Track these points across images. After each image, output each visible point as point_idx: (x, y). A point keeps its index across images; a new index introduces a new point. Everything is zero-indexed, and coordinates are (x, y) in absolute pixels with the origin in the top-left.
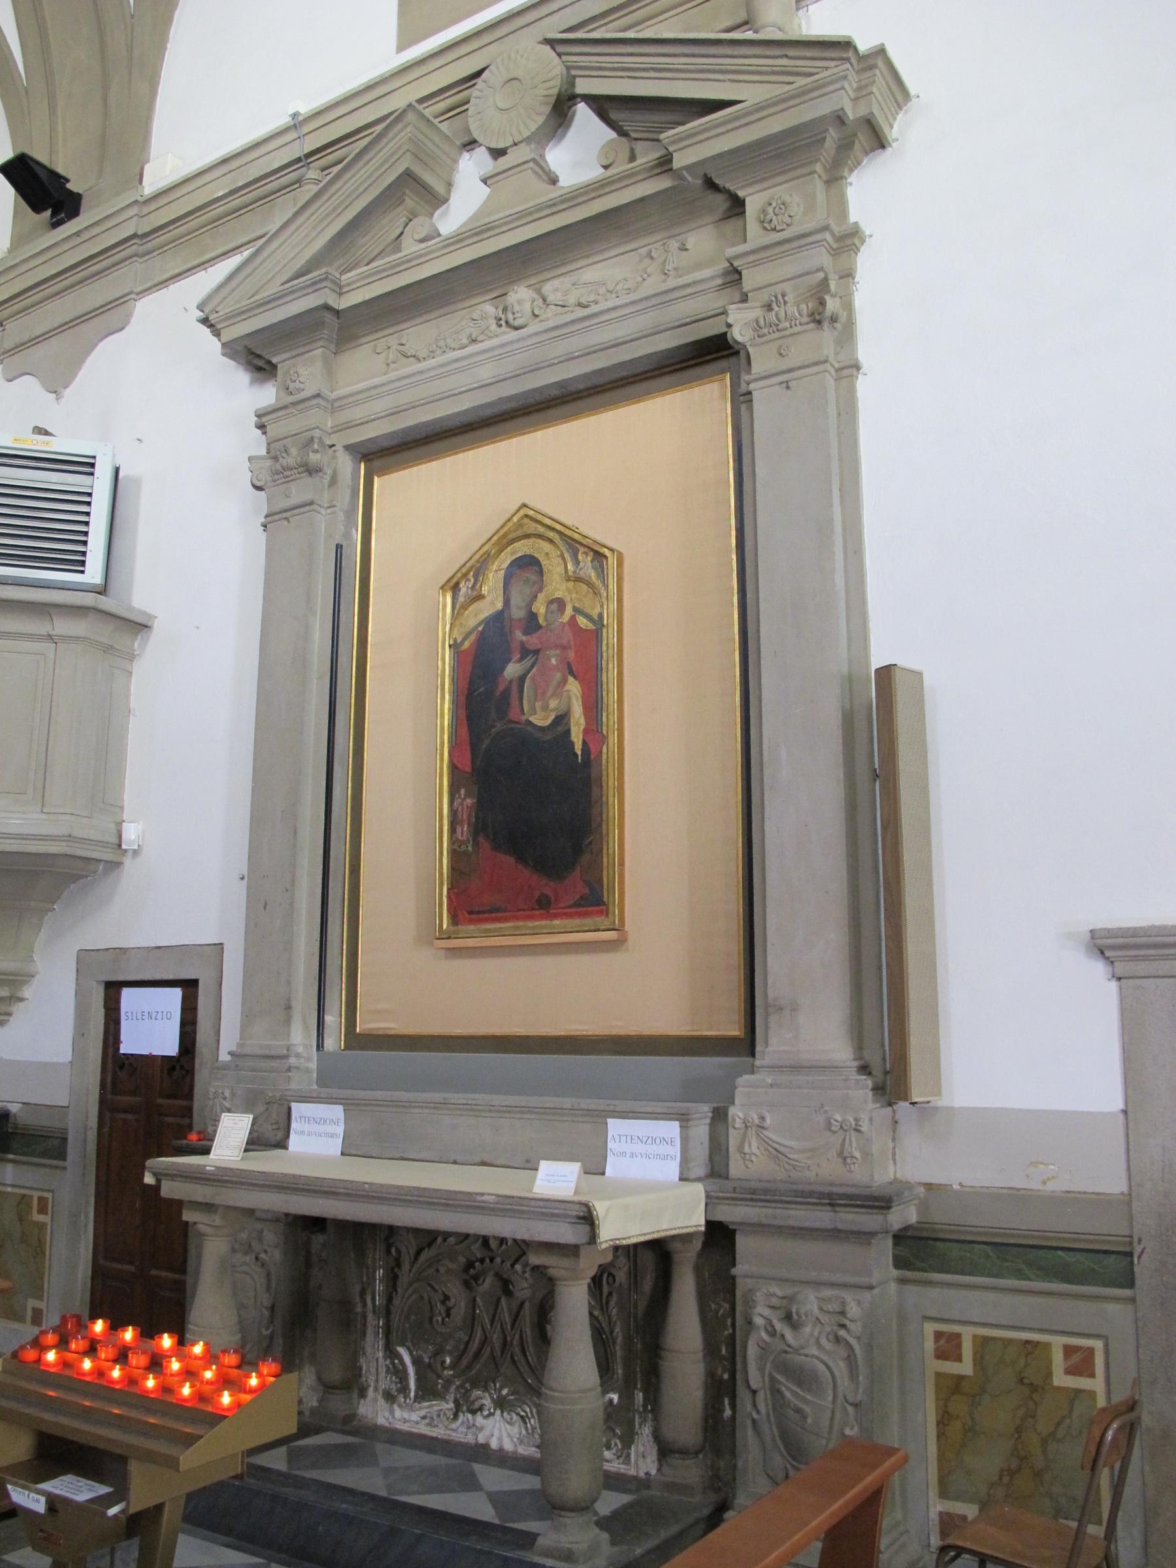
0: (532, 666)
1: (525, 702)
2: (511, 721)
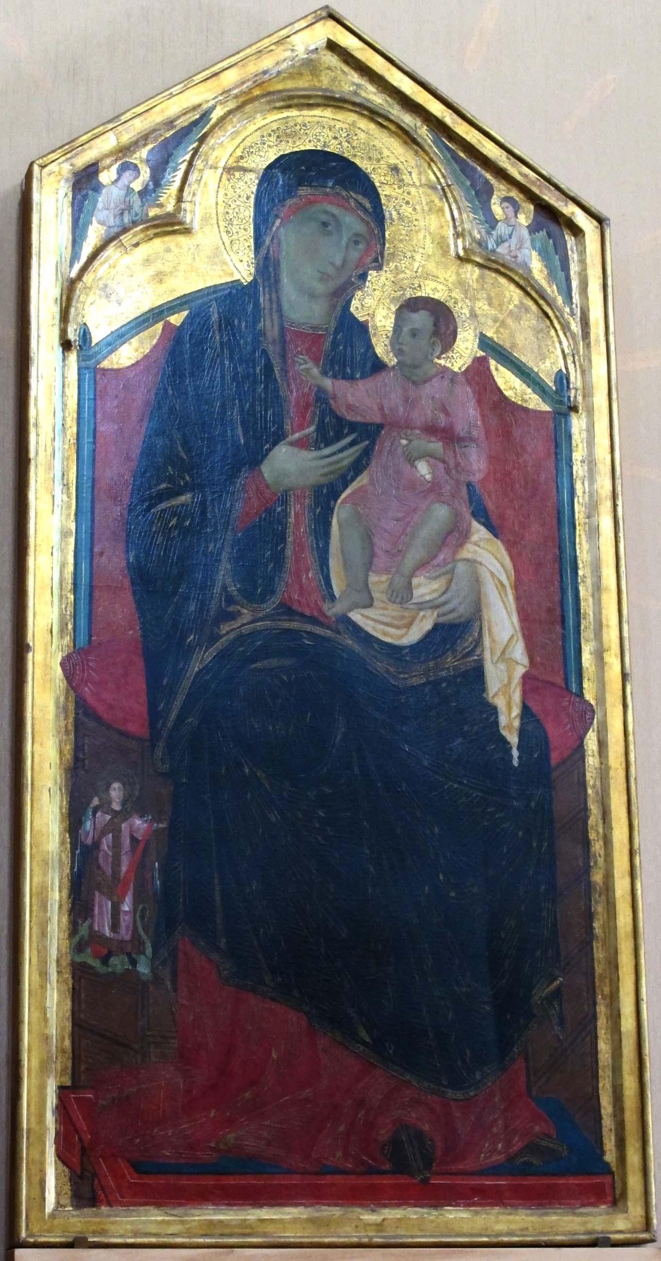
0: (358, 467)
2: (287, 610)
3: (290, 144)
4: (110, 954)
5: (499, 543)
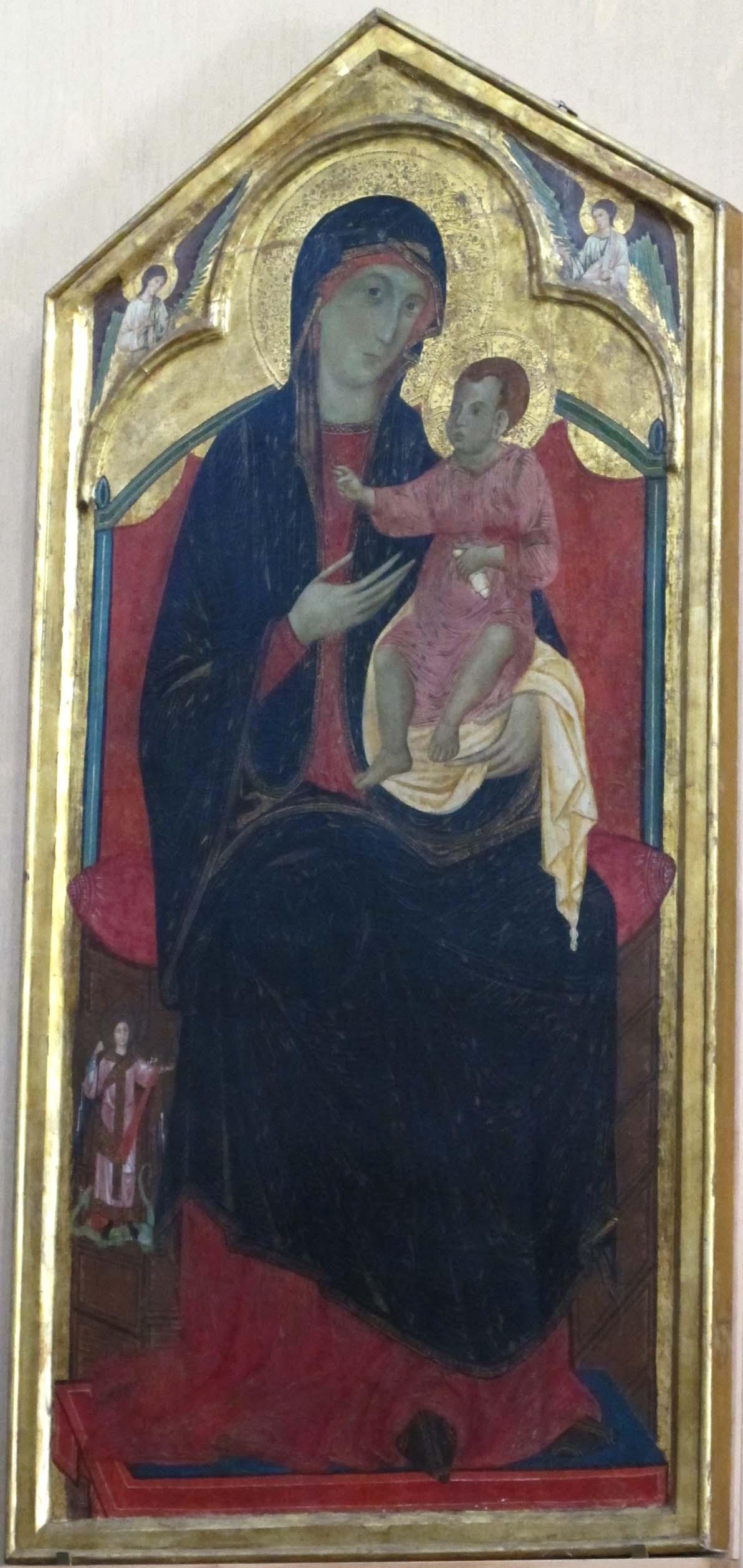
0: (400, 596)
2: (313, 791)
3: (337, 198)
4: (111, 1225)
5: (568, 663)
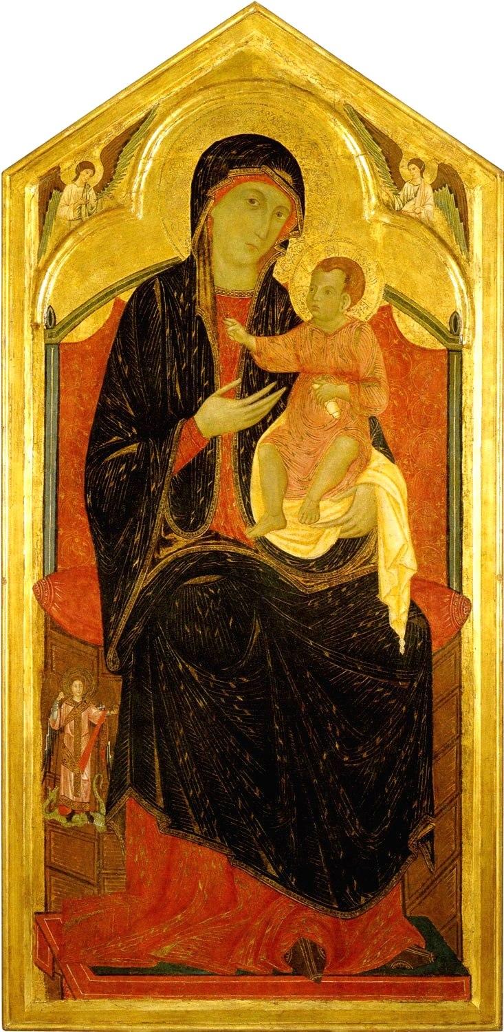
0: (275, 412)
1: (255, 495)
